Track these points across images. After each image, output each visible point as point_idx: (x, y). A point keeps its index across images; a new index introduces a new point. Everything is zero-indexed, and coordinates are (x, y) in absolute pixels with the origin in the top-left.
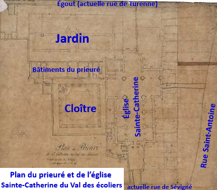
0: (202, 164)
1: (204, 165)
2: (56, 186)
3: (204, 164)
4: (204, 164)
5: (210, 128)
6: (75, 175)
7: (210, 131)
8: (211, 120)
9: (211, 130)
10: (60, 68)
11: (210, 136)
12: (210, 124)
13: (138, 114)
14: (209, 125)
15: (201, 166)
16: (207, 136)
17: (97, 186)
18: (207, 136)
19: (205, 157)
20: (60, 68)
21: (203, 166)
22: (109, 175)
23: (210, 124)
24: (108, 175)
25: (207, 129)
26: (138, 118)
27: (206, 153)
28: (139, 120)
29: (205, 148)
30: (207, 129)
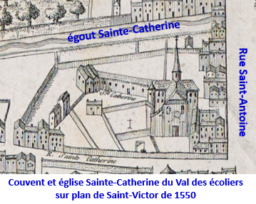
0: (246, 53)
1: (243, 52)
2: (242, 64)
3: (243, 54)
4: (243, 54)
5: (243, 103)
6: (57, 183)
7: (243, 100)
8: (242, 115)
9: (240, 102)
10: (106, 181)
11: (240, 93)
12: (242, 109)
13: (129, 33)
14: (244, 107)
15: (246, 49)
16: (245, 92)
17: (210, 183)
18: (245, 92)
19: (242, 64)
20: (106, 181)
21: (244, 51)
22: (242, 134)
23: (242, 109)
24: (243, 62)
25: (246, 102)
26: (124, 32)
27: (243, 68)
28: (122, 35)
29: (244, 74)
30: (246, 102)
